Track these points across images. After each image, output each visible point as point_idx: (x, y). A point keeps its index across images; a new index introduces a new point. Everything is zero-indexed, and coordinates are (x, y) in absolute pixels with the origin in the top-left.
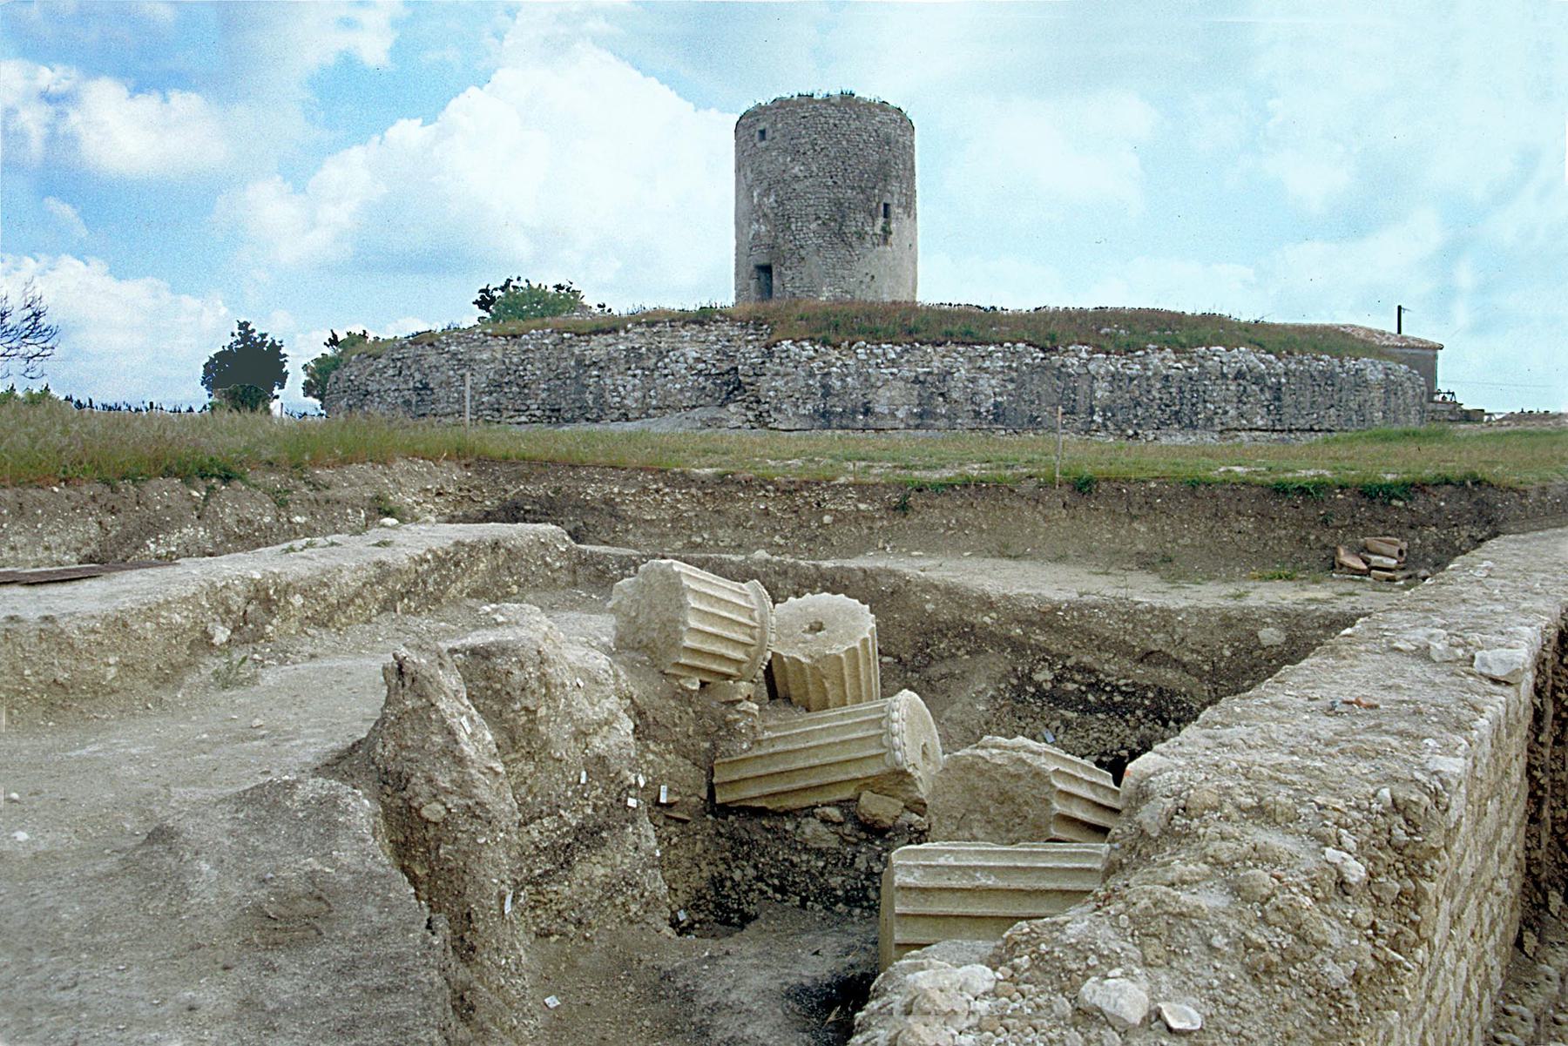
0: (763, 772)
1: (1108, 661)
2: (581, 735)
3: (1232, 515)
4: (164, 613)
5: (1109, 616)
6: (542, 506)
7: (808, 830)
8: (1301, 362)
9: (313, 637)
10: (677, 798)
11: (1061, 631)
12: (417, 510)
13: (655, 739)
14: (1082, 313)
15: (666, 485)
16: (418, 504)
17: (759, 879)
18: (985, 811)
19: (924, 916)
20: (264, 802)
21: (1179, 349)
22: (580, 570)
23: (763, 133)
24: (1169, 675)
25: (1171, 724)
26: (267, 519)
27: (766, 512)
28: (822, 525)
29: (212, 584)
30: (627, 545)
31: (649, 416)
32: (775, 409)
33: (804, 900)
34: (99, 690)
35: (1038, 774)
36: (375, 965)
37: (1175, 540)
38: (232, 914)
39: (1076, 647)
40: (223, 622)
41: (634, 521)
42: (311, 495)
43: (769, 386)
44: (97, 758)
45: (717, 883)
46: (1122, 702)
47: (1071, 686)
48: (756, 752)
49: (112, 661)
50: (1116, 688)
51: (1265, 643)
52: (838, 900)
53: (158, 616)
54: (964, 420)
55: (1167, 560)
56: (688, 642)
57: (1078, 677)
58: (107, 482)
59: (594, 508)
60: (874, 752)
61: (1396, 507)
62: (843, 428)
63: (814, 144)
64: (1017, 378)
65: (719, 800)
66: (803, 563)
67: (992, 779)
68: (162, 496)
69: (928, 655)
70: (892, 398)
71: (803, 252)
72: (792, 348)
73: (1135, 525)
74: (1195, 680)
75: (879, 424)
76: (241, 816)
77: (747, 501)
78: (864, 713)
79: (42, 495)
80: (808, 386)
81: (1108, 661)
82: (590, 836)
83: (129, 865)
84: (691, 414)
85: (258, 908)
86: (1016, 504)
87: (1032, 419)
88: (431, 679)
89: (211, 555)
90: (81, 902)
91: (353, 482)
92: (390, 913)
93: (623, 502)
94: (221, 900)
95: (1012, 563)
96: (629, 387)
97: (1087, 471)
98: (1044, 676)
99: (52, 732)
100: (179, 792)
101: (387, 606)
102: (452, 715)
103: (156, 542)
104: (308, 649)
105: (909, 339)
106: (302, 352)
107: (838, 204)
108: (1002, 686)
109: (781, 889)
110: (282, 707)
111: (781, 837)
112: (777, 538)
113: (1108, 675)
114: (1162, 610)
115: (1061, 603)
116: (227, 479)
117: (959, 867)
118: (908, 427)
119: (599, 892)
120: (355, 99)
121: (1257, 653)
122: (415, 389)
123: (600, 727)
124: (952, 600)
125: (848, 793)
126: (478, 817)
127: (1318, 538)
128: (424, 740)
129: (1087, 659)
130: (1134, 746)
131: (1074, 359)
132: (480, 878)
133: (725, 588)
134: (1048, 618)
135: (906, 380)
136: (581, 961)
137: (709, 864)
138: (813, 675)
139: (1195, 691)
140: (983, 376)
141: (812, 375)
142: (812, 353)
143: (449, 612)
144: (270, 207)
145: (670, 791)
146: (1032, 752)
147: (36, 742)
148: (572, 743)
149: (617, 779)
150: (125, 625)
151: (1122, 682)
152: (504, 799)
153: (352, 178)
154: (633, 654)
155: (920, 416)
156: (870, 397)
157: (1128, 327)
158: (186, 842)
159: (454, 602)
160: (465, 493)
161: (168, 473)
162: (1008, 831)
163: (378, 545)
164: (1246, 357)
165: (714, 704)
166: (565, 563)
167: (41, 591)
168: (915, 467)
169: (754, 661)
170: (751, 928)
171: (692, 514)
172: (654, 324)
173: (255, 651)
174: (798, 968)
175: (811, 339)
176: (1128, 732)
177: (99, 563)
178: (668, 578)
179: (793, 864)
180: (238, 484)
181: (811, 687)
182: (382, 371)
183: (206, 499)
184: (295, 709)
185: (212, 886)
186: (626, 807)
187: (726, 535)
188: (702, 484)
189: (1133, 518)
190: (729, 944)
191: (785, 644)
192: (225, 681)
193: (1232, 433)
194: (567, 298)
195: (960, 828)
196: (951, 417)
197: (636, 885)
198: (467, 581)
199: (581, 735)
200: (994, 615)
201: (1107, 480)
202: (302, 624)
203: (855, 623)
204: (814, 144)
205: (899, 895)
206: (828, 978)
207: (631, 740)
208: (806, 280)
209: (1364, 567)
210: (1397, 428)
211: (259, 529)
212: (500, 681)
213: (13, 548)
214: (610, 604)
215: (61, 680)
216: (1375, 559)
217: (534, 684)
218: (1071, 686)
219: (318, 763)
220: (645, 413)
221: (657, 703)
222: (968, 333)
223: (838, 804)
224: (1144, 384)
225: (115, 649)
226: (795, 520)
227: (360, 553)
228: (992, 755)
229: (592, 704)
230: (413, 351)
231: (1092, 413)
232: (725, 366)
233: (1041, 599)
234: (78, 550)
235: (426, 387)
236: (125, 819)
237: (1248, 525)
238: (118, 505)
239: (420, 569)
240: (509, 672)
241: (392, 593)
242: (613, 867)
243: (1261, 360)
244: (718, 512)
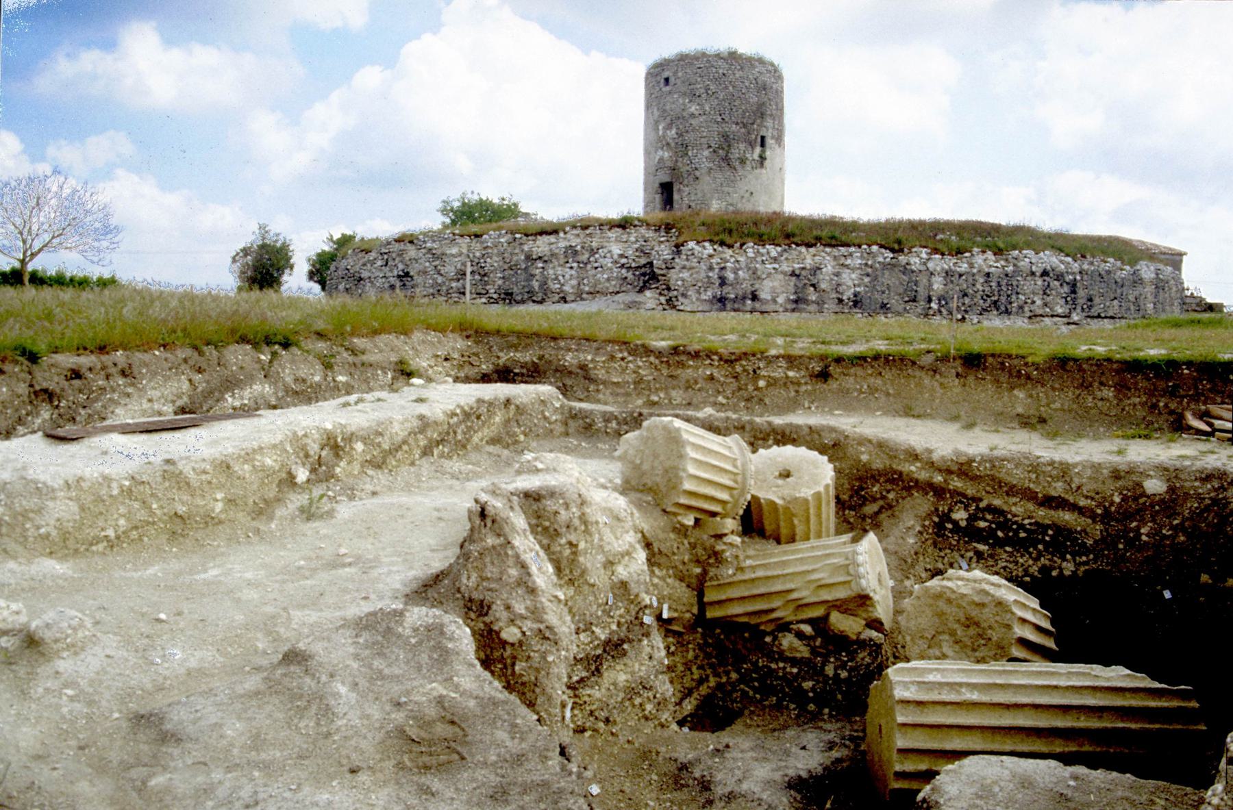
0: (746, 594)
1: (1015, 504)
2: (609, 564)
3: (1096, 384)
4: (258, 457)
5: (1016, 467)
6: (528, 370)
8: (1092, 263)
9: (372, 477)
10: (676, 615)
11: (975, 478)
12: (430, 371)
13: (659, 565)
14: (922, 223)
16: (431, 367)
18: (952, 633)
19: (922, 726)
20: (377, 628)
21: (998, 252)
22: (571, 422)
23: (667, 80)
24: (1067, 517)
25: (1068, 557)
26: (317, 378)
27: (712, 378)
28: (757, 389)
29: (295, 433)
31: (582, 299)
32: (683, 295)
34: (210, 521)
35: (1000, 604)
36: (525, 792)
37: (1048, 405)
38: (380, 736)
39: (988, 492)
40: (304, 464)
41: (604, 383)
42: (351, 359)
43: (677, 277)
44: (220, 582)
47: (982, 524)
48: (740, 577)
49: (219, 496)
50: (1021, 527)
51: (1149, 491)
53: (254, 459)
54: (831, 306)
55: (1043, 421)
56: (688, 485)
57: (989, 517)
58: (196, 348)
59: (570, 373)
60: (841, 579)
62: (735, 310)
63: (707, 89)
64: (871, 273)
66: (758, 420)
67: (959, 606)
68: (237, 358)
69: (863, 497)
70: (775, 288)
71: (698, 174)
72: (697, 248)
74: (1089, 521)
75: (764, 308)
76: (361, 640)
79: (147, 357)
80: (708, 277)
81: (1015, 504)
82: (615, 648)
83: (272, 687)
84: (617, 298)
85: (401, 731)
86: (918, 373)
87: (883, 306)
88: (506, 520)
89: (275, 407)
90: (239, 718)
91: (381, 349)
92: (522, 739)
93: (595, 368)
94: (365, 722)
95: (918, 422)
96: (567, 277)
97: (976, 348)
98: (960, 515)
99: (176, 556)
100: (297, 614)
101: (427, 452)
102: (525, 551)
103: (233, 396)
104: (369, 487)
105: (787, 242)
106: (306, 246)
107: (725, 136)
110: (360, 537)
113: (1015, 516)
114: (1061, 463)
115: (975, 456)
116: (286, 345)
117: (948, 684)
118: (786, 310)
119: (622, 695)
120: (328, 55)
121: (1142, 500)
122: (399, 276)
123: (623, 556)
124: (884, 452)
125: (818, 612)
127: (1166, 406)
128: (501, 573)
129: (997, 502)
131: (917, 258)
132: (549, 690)
133: (713, 441)
134: (964, 469)
135: (784, 273)
138: (784, 513)
139: (1088, 530)
140: (844, 271)
141: (711, 268)
142: (711, 251)
143: (474, 456)
144: (267, 133)
145: (670, 608)
146: (993, 584)
147: (165, 566)
148: (603, 571)
149: (634, 601)
150: (228, 467)
151: (1026, 522)
153: (329, 118)
154: (639, 495)
155: (796, 302)
156: (757, 286)
157: (958, 234)
158: (320, 664)
159: (477, 448)
160: (466, 359)
161: (244, 340)
162: (974, 650)
163: (416, 401)
164: (1050, 259)
165: (705, 537)
167: (155, 437)
168: (829, 343)
169: (737, 501)
171: (650, 378)
172: (586, 228)
173: (328, 489)
174: (792, 762)
175: (711, 241)
176: (1031, 562)
177: (191, 414)
178: (670, 432)
180: (294, 349)
182: (373, 262)
183: (271, 362)
184: (371, 540)
185: (357, 712)
186: (642, 624)
188: (659, 354)
191: (761, 488)
192: (308, 514)
193: (1038, 319)
194: (511, 211)
195: (932, 647)
196: (820, 303)
197: (651, 688)
198: (486, 431)
199: (609, 564)
201: (993, 355)
202: (362, 466)
203: (817, 475)
204: (707, 89)
205: (898, 708)
207: (646, 568)
208: (700, 195)
209: (1208, 429)
210: (1163, 316)
211: (311, 386)
212: (549, 520)
213: (150, 400)
214: (617, 454)
215: (180, 512)
216: (1218, 423)
217: (576, 522)
218: (982, 524)
219: (408, 590)
220: (580, 296)
221: (661, 536)
222: (833, 238)
224: (970, 279)
225: (221, 487)
227: (403, 407)
228: (958, 586)
229: (617, 538)
230: (396, 247)
231: (930, 301)
232: (643, 261)
233: (957, 453)
234: (173, 402)
235: (407, 274)
236: (257, 639)
237: (1109, 393)
238: (204, 366)
239: (452, 421)
240: (556, 513)
241: (430, 440)
242: (633, 673)
243: (1061, 262)
244: (671, 376)
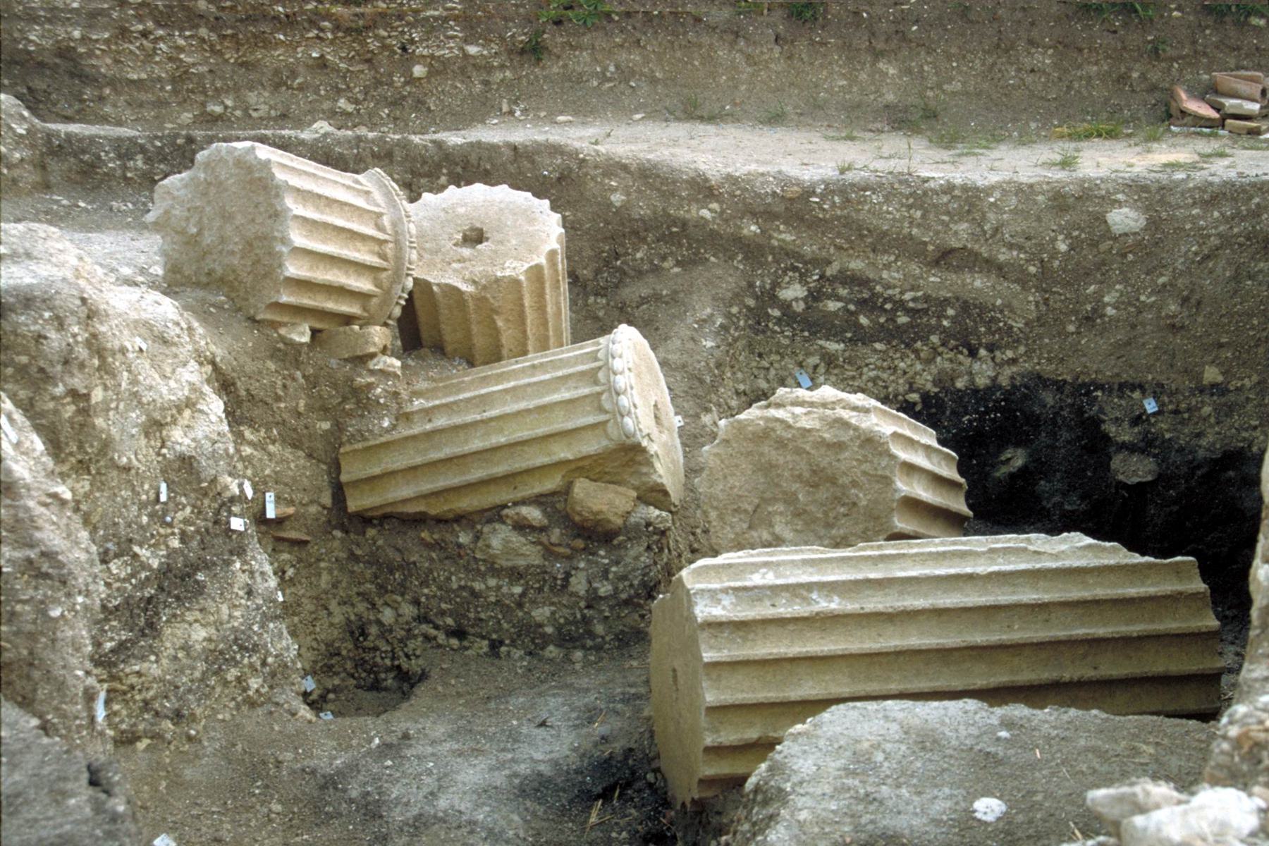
0: (419, 460)
3: (1021, 45)
5: (887, 199)
7: (496, 542)
10: (291, 510)
13: (251, 423)
15: (159, 24)
17: (423, 619)
18: (790, 499)
22: (53, 164)
24: (978, 282)
25: (983, 352)
27: (322, 63)
28: (411, 80)
30: (104, 120)
33: (495, 646)
39: (839, 248)
41: (112, 82)
45: (357, 631)
46: (910, 325)
47: (833, 306)
50: (900, 305)
52: (546, 640)
55: (931, 115)
56: (294, 269)
57: (843, 292)
59: (42, 65)
60: (591, 420)
61: (1255, 27)
65: (353, 505)
66: (416, 139)
67: (799, 451)
73: (881, 65)
77: (292, 46)
78: (554, 365)
81: (887, 266)
82: (179, 583)
86: (706, 40)
95: (711, 129)
98: (793, 292)
108: (735, 310)
109: (460, 633)
111: (456, 555)
112: (342, 103)
113: (888, 286)
114: (965, 188)
115: (813, 185)
117: (786, 588)
119: (201, 666)
121: (1103, 247)
123: (180, 411)
124: (652, 187)
125: (551, 483)
126: (47, 576)
127: (1143, 76)
129: (856, 265)
130: (929, 386)
132: (58, 672)
133: (334, 183)
134: (795, 206)
136: (188, 773)
137: (343, 603)
139: (1015, 303)
145: (278, 499)
148: (143, 442)
149: (211, 490)
151: (908, 296)
152: (77, 543)
154: (201, 294)
162: (829, 526)
165: (334, 363)
166: (26, 153)
169: (388, 292)
170: (421, 689)
171: (203, 69)
174: (525, 751)
176: (919, 367)
179: (473, 593)
181: (475, 329)
186: (229, 531)
187: (261, 101)
189: (878, 55)
190: (401, 720)
191: (431, 265)
195: (755, 528)
197: (255, 648)
199: (155, 427)
200: (715, 206)
203: (532, 233)
205: (703, 636)
206: (574, 761)
209: (1214, 114)
212: (26, 351)
214: (150, 217)
216: (1230, 103)
217: (82, 352)
218: (833, 306)
221: (250, 367)
223: (538, 500)
226: (368, 74)
229: (165, 377)
233: (784, 181)
237: (1045, 59)
242: (218, 625)
244: (242, 64)
